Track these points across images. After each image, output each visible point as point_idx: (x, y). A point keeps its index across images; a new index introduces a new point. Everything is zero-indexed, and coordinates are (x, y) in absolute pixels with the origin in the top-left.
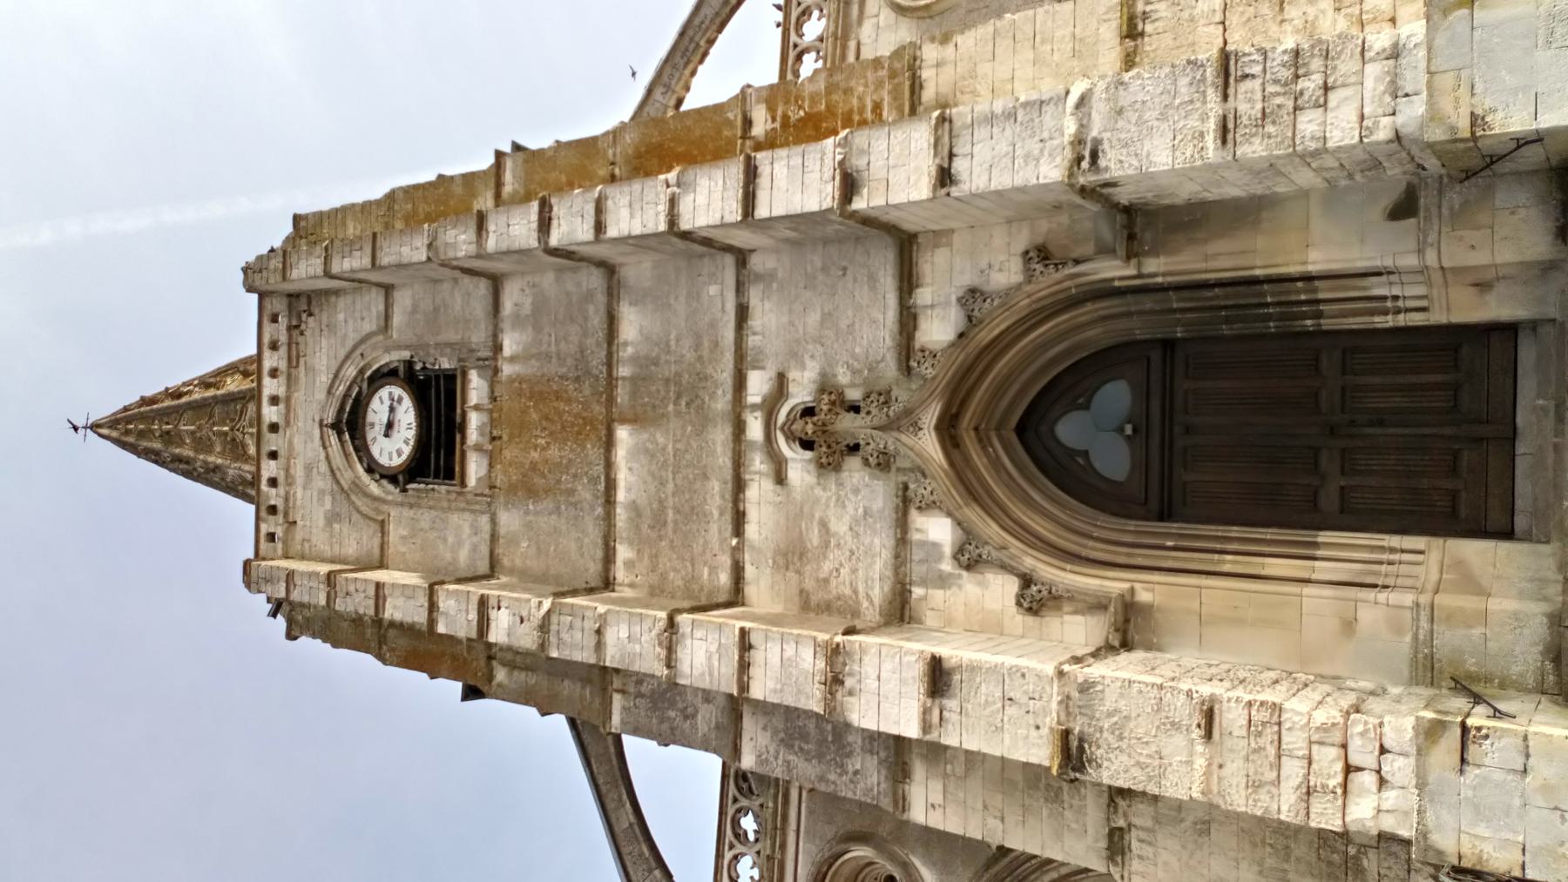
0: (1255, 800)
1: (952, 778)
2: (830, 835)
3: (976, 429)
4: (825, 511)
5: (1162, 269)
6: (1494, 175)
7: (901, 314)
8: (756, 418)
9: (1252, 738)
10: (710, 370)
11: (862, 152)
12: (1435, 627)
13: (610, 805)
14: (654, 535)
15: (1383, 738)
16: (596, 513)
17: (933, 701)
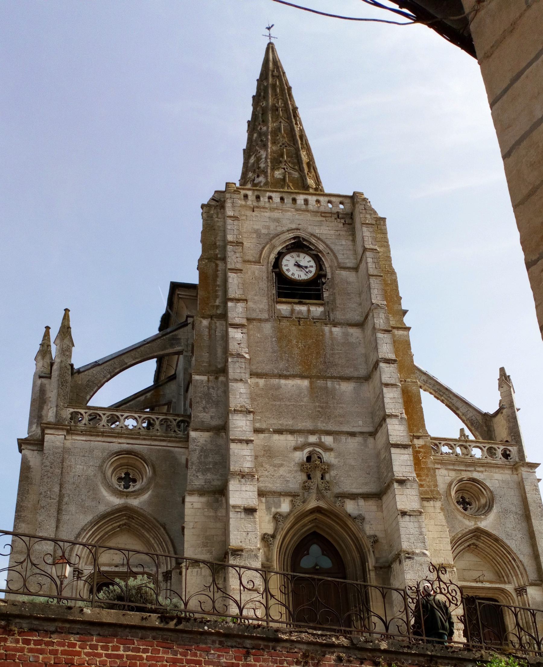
3: (316, 519)
5: (371, 577)
7: (356, 494)
8: (316, 439)
10: (332, 421)
13: (133, 353)
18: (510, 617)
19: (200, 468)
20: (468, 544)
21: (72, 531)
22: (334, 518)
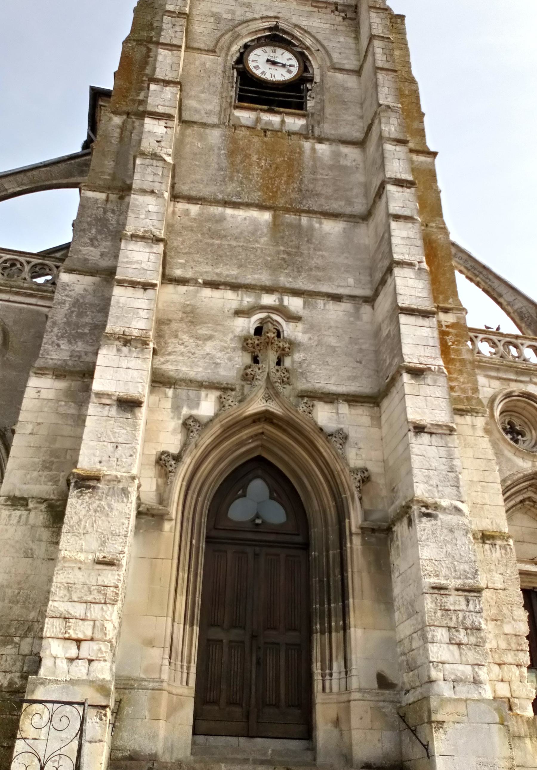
0: (60, 587)
1: (57, 405)
2: (6, 321)
3: (263, 433)
4: (219, 339)
5: (354, 547)
6: (400, 731)
7: (334, 394)
8: (275, 301)
9: (97, 587)
10: (304, 275)
11: (435, 381)
12: (149, 691)
13: (19, 177)
14: (205, 230)
15: (97, 662)
16: (219, 194)
17: (114, 400)
19: (66, 332)
20: (521, 498)
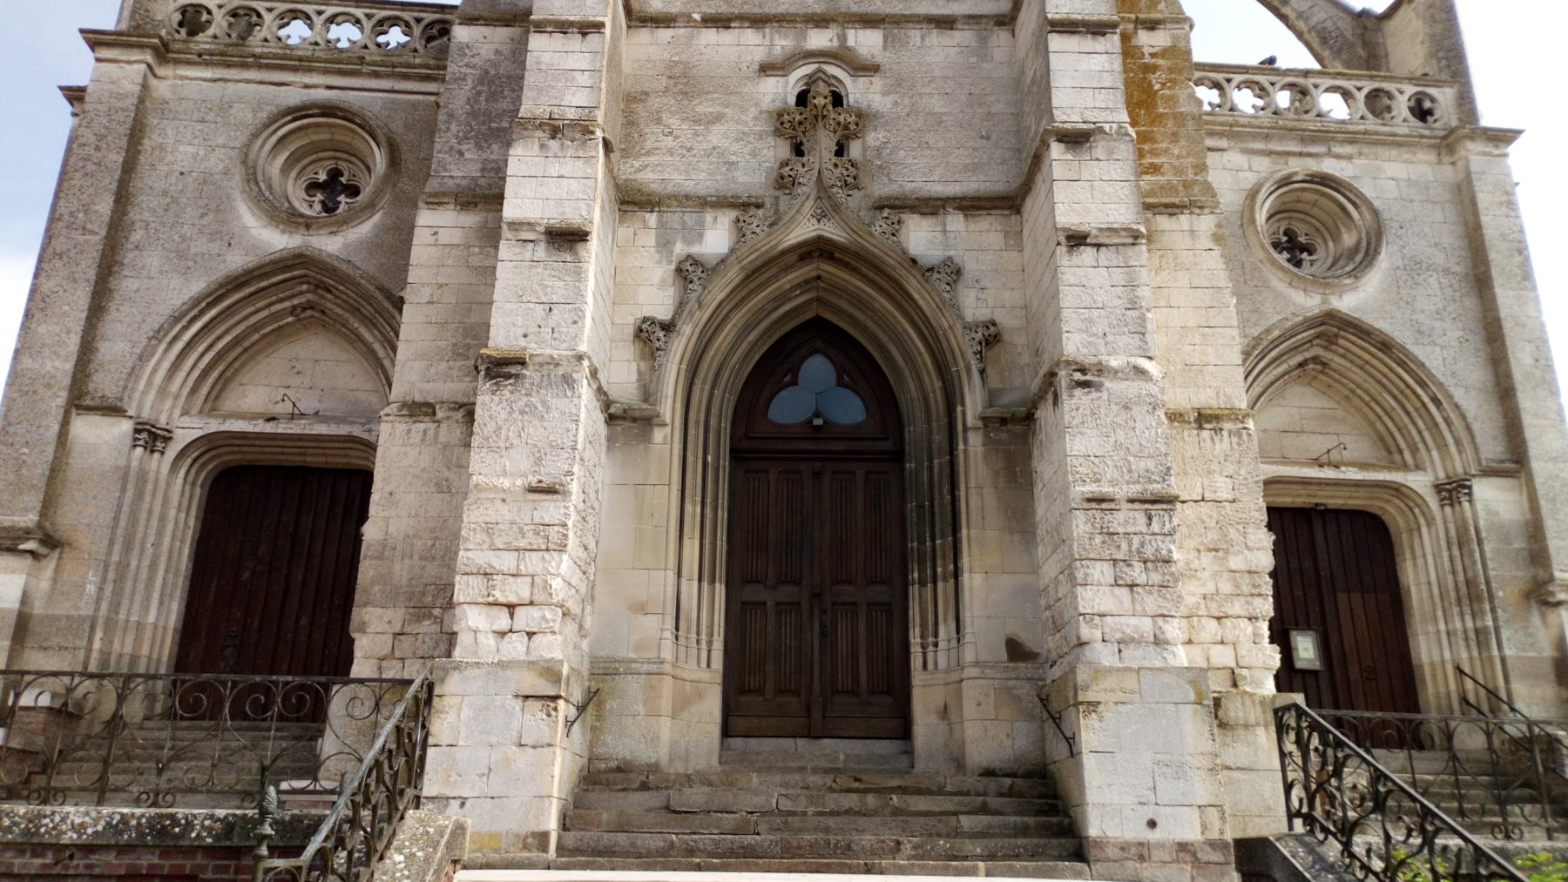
0: (474, 530)
2: (393, 126)
3: (819, 278)
5: (971, 449)
8: (831, 40)
11: (1111, 152)
18: (1415, 565)
19: (472, 130)
20: (1299, 358)
21: (144, 321)
22: (872, 275)
